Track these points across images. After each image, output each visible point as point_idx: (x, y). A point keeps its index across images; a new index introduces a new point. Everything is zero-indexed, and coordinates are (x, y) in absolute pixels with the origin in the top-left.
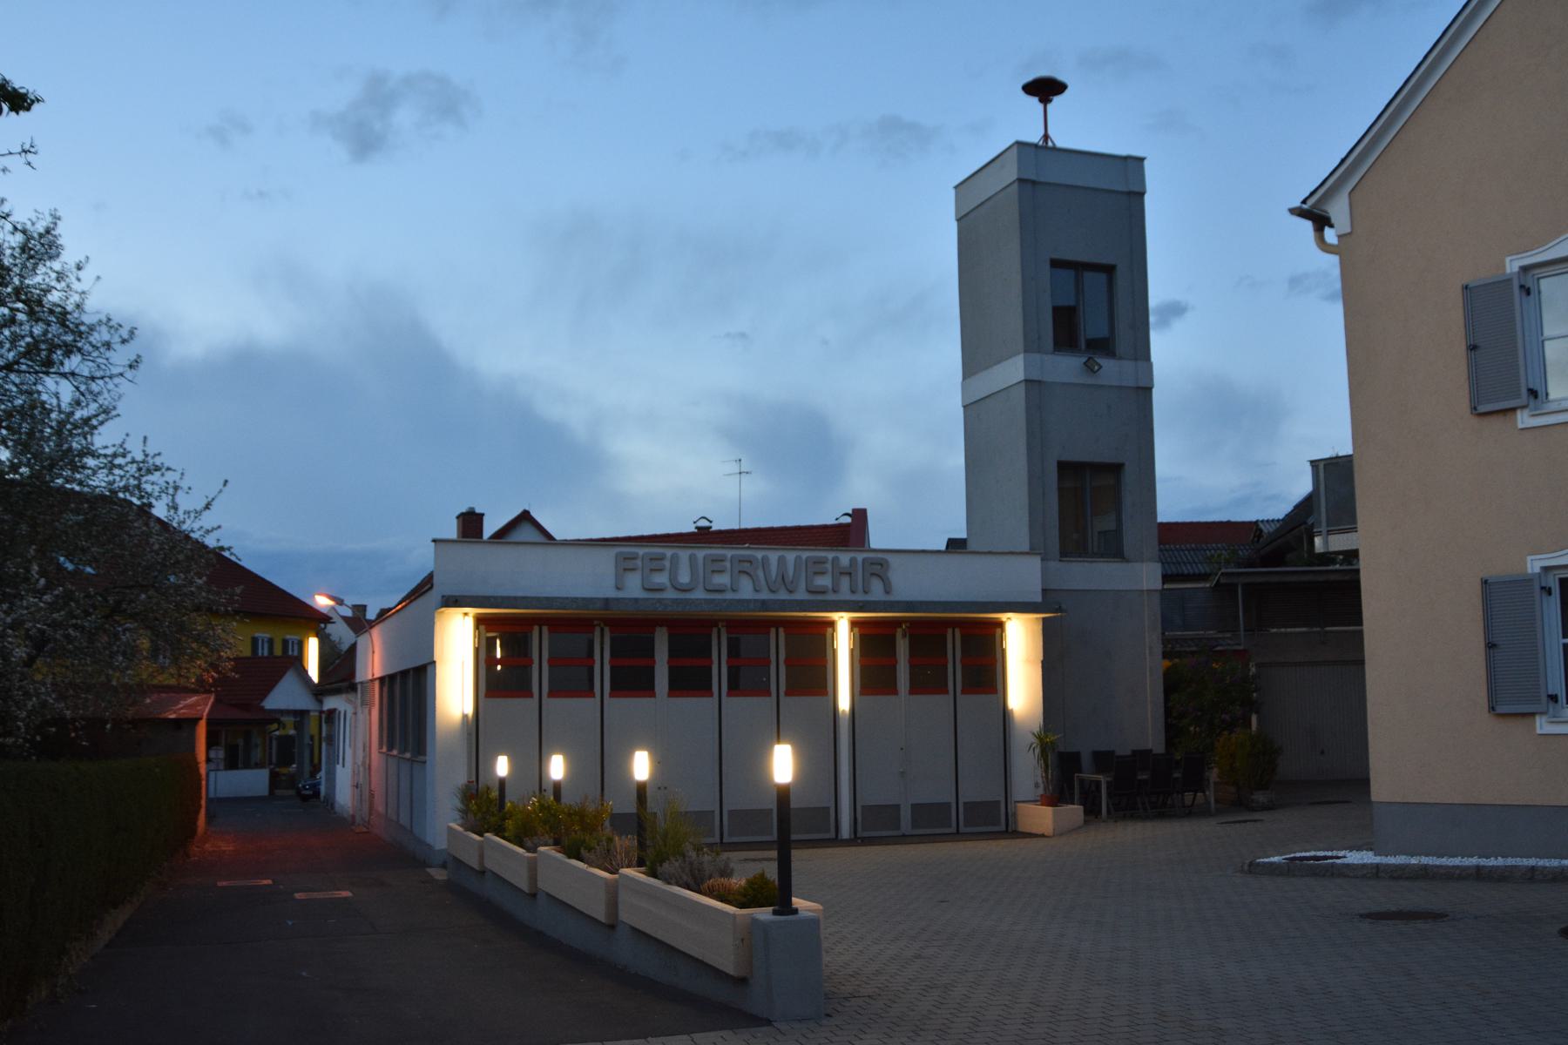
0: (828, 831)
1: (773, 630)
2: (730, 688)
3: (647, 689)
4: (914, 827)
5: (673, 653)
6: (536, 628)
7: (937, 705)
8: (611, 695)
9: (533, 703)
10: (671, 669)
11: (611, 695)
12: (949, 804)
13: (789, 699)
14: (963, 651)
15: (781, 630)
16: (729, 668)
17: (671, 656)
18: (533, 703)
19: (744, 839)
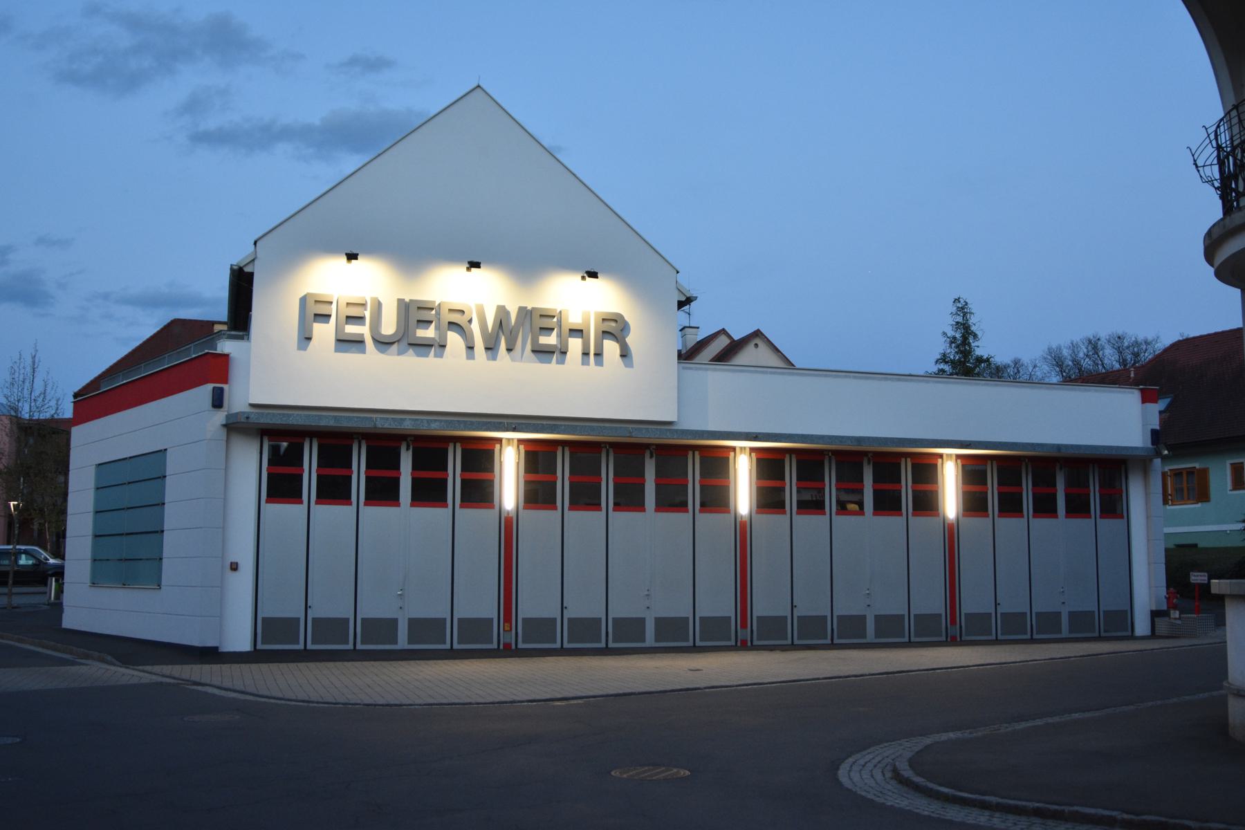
0: (730, 639)
1: (690, 454)
2: (914, 509)
3: (639, 506)
4: (657, 640)
5: (876, 480)
6: (560, 449)
7: (679, 520)
8: (317, 503)
9: (989, 521)
10: (875, 491)
11: (366, 504)
12: (347, 620)
13: (618, 514)
14: (837, 480)
15: (697, 453)
16: (702, 487)
17: (414, 468)
18: (1023, 521)
19: (1119, 634)
